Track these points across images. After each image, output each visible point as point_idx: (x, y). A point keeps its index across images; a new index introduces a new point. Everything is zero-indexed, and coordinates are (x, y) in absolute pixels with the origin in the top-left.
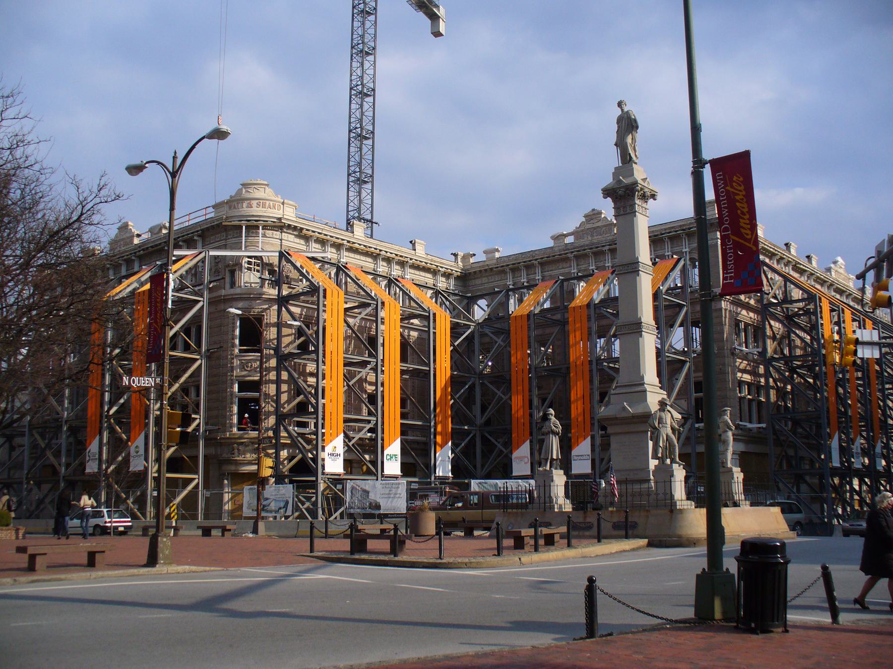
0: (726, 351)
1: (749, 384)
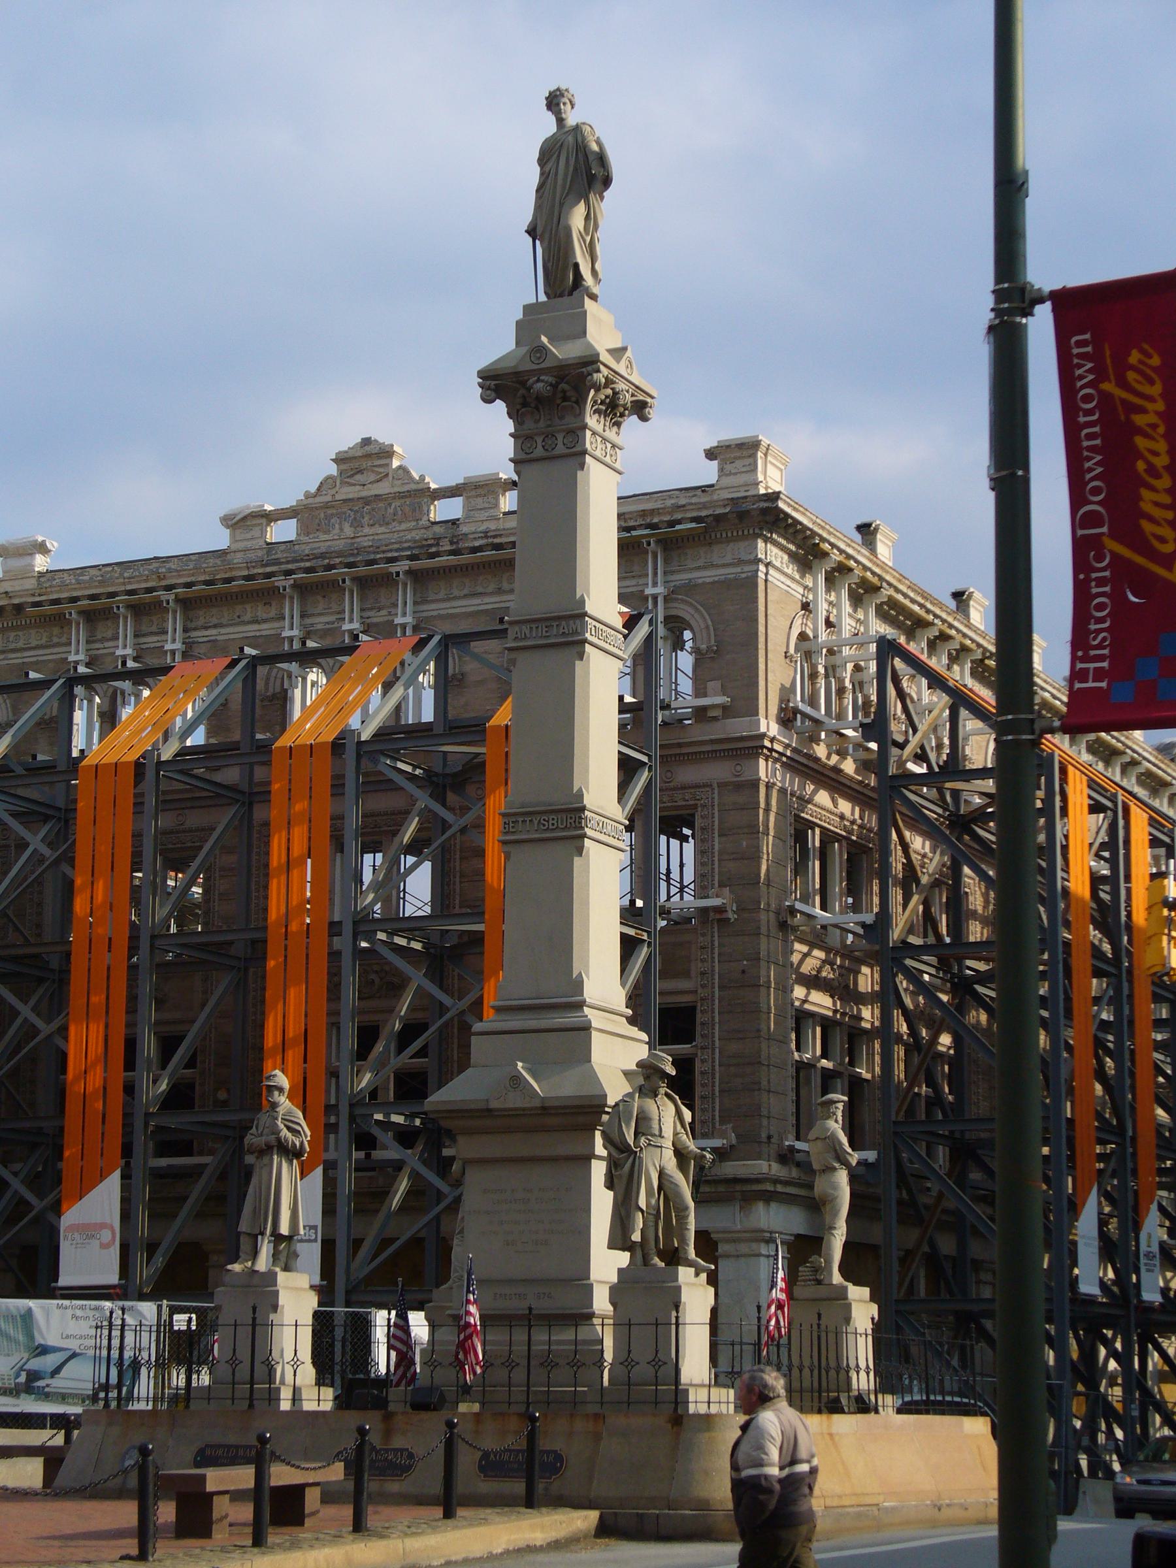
0: (763, 917)
1: (827, 1024)
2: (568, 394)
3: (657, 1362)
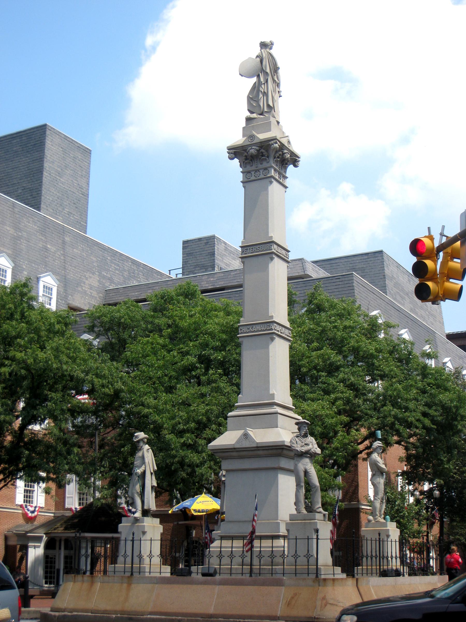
2: (264, 154)
3: (308, 556)
